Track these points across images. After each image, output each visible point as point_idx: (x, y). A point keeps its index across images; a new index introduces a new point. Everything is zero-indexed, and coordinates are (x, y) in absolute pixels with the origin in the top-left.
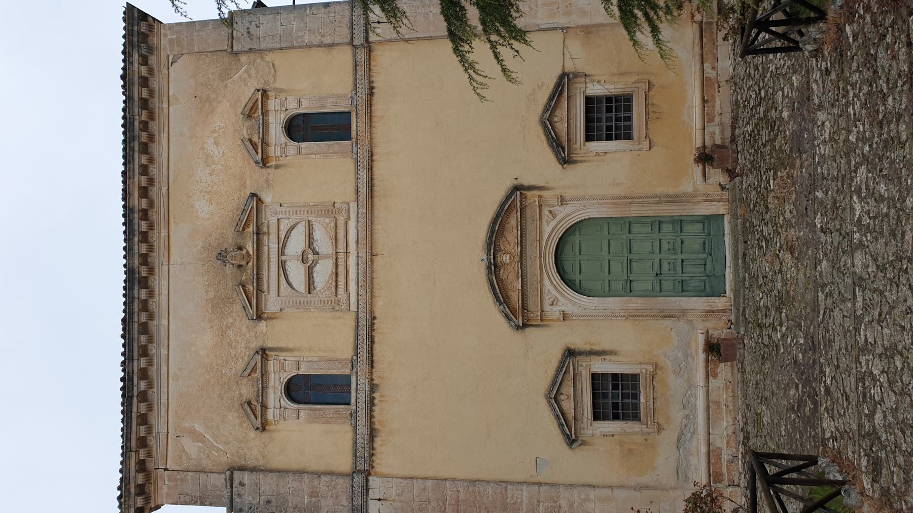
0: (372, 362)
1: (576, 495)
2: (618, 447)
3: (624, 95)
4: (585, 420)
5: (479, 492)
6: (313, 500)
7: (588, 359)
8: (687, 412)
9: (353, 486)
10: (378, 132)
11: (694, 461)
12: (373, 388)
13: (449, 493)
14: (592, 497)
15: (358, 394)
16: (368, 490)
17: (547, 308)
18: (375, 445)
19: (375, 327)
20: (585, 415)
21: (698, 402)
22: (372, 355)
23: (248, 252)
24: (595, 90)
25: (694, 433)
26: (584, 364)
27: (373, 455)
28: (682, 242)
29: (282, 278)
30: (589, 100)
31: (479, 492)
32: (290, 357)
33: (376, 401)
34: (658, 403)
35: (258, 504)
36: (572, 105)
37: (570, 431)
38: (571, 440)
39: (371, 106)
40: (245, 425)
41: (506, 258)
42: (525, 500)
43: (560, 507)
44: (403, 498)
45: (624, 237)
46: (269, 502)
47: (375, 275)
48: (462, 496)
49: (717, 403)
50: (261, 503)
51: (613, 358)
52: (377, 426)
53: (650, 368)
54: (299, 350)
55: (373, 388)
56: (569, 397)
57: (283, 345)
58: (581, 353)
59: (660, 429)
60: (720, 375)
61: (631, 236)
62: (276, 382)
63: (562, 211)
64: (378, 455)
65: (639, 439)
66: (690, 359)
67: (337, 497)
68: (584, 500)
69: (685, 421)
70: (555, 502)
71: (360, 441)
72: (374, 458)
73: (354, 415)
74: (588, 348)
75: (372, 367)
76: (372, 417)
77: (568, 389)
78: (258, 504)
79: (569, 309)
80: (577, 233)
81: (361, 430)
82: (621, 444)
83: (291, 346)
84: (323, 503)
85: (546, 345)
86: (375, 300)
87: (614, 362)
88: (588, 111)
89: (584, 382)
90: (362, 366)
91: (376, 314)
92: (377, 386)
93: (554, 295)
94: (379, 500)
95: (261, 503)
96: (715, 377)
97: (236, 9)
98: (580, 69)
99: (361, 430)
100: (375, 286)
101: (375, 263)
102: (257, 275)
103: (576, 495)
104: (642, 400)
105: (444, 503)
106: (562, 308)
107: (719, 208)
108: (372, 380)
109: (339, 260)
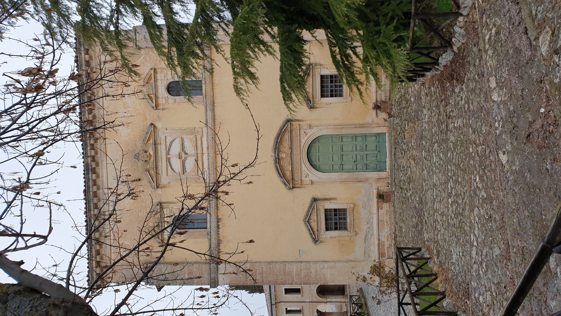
0: (218, 207)
1: (318, 267)
8: (369, 226)
10: (217, 91)
11: (372, 248)
12: (218, 220)
14: (326, 267)
16: (218, 270)
17: (304, 179)
23: (150, 154)
33: (220, 227)
34: (356, 221)
41: (284, 155)
48: (264, 270)
49: (383, 221)
52: (221, 239)
53: (352, 206)
55: (218, 220)
56: (314, 221)
58: (320, 200)
59: (356, 234)
61: (342, 143)
65: (347, 239)
73: (209, 234)
74: (323, 197)
75: (218, 210)
76: (218, 234)
79: (314, 179)
81: (213, 241)
85: (303, 197)
87: (335, 203)
92: (220, 219)
93: (307, 172)
96: (382, 209)
98: (318, 62)
99: (213, 241)
103: (318, 267)
104: (348, 220)
106: (311, 179)
107: (384, 130)
108: (218, 216)
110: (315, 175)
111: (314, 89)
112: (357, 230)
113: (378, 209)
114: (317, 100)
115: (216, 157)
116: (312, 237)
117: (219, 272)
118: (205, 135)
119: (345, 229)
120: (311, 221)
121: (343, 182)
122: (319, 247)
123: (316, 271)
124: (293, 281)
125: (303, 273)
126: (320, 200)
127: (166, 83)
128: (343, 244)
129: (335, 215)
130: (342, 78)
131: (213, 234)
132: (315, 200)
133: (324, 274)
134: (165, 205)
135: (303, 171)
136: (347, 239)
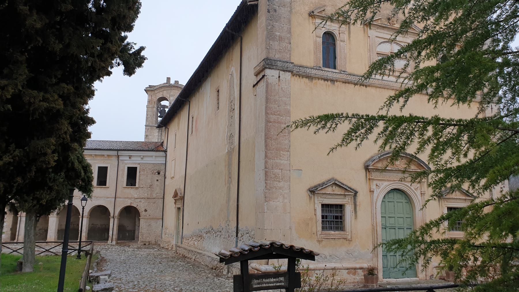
0: (345, 83)
1: (286, 191)
2: (309, 217)
3: (344, 226)
4: (322, 199)
5: (285, 136)
6: (278, 38)
7: (353, 203)
8: (328, 257)
9: (287, 62)
12: (333, 81)
14: (286, 201)
15: (329, 73)
16: (284, 71)
17: (375, 182)
18: (304, 78)
19: (362, 87)
20: (325, 200)
21: (333, 264)
22: (349, 83)
23: (395, 24)
24: (348, 210)
27: (299, 77)
29: (383, 40)
30: (341, 207)
31: (285, 136)
32: (345, 37)
33: (326, 82)
34: (332, 241)
35: (274, 4)
36: (462, 201)
37: (319, 190)
38: (313, 191)
40: (312, 5)
42: (282, 162)
45: (405, 226)
46: (275, 11)
47: (386, 90)
50: (275, 6)
51: (353, 217)
52: (314, 81)
53: (349, 237)
54: (350, 43)
55: (333, 81)
56: (333, 191)
57: (352, 34)
58: (355, 199)
59: (319, 242)
60: (348, 275)
61: (405, 229)
62: (333, 27)
63: (418, 193)
64: (299, 80)
65: (314, 230)
66: (354, 259)
67: (280, 52)
68: (284, 196)
69: (323, 256)
70: (282, 179)
71: (308, 71)
72: (298, 77)
73: (319, 69)
74: (358, 204)
75: (343, 82)
76: (319, 79)
77: (338, 191)
78: (274, 4)
79: (375, 194)
80: (406, 201)
81: (314, 72)
83: (351, 39)
84: (276, 43)
85: (356, 180)
86: (375, 88)
87: (351, 218)
88: (337, 206)
89: (339, 200)
90: (344, 77)
91: (368, 88)
92: (334, 84)
93: (384, 185)
94: (279, 77)
95: (275, 6)
96: (348, 273)
99: (314, 72)
100: (381, 89)
101: (391, 91)
102: (386, 27)
103: (286, 191)
104: (333, 232)
105: (278, 115)
106: (375, 190)
108: (337, 81)
110: (380, 193)
111: (458, 201)
112: (324, 243)
114: (446, 203)
115: (393, 89)
116: (319, 185)
117: (281, 72)
119: (323, 228)
120: (334, 187)
121: (374, 230)
122: (304, 194)
123: (280, 188)
124: (270, 159)
126: (355, 199)
127: (336, 33)
129: (337, 217)
131: (319, 73)
132: (356, 193)
133: (277, 198)
134: (347, 28)
135: (383, 182)
136: (314, 230)
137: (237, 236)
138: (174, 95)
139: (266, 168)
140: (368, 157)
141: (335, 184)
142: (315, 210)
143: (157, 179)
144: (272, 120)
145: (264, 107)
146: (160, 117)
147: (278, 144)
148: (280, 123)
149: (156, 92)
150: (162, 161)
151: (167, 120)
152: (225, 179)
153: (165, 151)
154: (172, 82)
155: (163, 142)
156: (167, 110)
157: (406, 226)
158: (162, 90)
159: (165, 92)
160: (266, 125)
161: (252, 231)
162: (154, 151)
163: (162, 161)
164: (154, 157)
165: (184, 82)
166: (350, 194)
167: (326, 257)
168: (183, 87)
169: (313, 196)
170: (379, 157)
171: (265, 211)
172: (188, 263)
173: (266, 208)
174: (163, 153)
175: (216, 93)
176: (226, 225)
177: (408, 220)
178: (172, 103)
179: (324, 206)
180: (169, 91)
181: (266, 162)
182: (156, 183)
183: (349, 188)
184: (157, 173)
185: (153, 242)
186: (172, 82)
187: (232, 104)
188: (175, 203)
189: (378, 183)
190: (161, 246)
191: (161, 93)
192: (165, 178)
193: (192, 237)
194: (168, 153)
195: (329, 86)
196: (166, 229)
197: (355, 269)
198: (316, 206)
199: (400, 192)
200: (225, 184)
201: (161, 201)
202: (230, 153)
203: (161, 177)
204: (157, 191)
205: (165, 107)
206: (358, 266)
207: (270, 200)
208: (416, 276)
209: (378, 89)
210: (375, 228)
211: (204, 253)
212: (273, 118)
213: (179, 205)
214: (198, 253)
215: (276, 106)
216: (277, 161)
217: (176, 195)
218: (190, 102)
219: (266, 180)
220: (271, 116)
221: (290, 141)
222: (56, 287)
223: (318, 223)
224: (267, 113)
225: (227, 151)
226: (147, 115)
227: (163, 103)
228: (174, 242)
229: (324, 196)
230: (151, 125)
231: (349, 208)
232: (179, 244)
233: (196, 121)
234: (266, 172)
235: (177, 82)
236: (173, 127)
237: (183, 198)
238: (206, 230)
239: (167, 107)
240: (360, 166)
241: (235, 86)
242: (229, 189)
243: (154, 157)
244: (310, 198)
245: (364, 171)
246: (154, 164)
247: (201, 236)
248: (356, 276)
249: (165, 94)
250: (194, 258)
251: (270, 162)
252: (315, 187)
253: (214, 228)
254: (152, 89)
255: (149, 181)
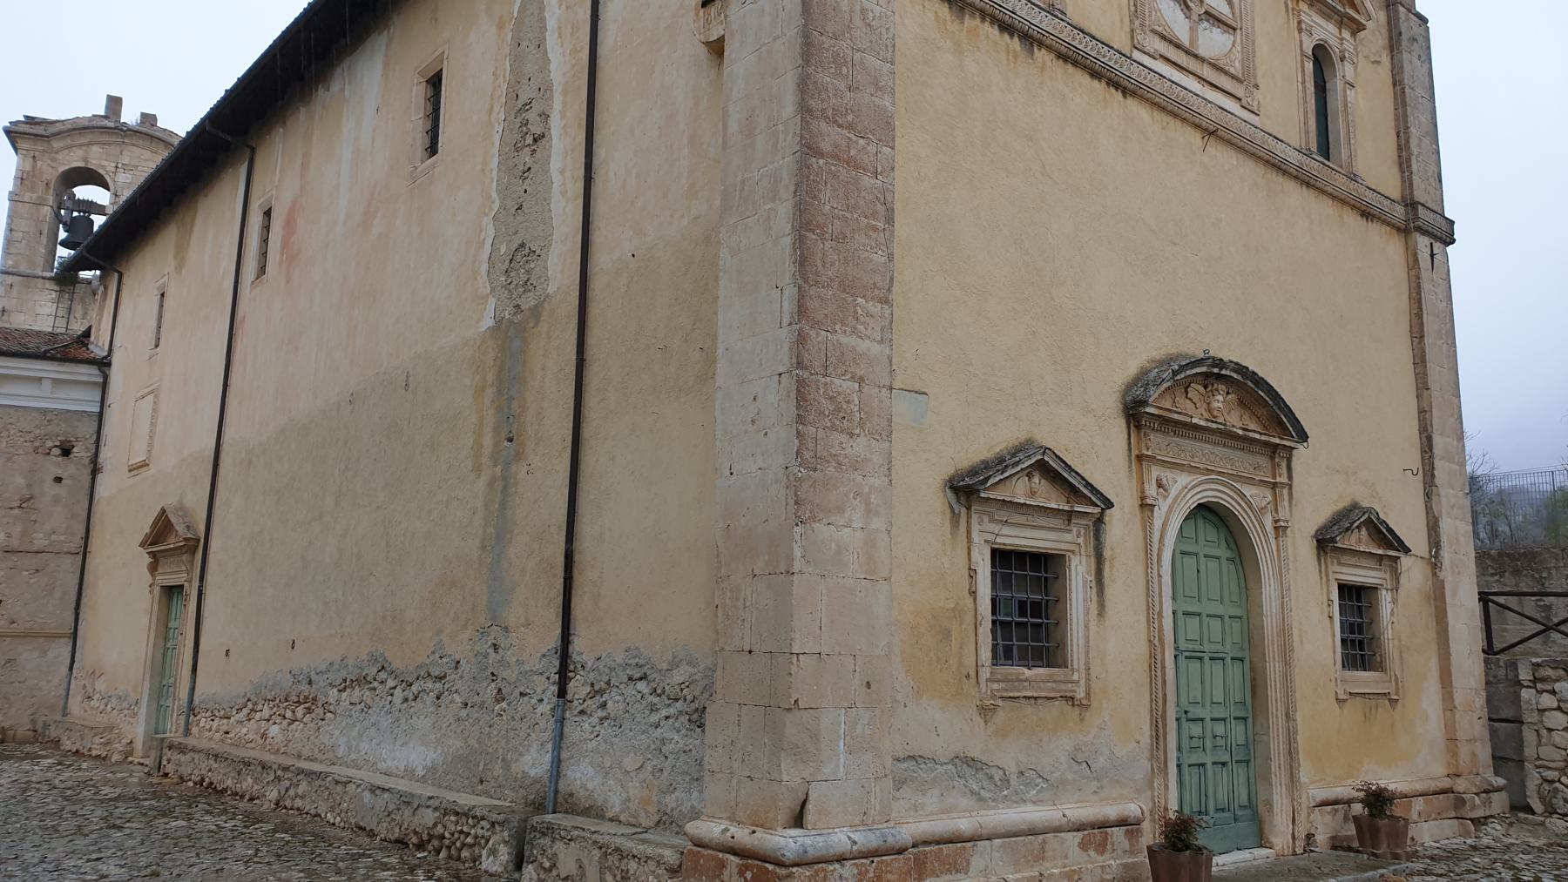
5: (875, 229)
10: (1327, 208)
11: (931, 800)
13: (872, 149)
14: (877, 524)
17: (1156, 471)
20: (1006, 530)
21: (1030, 807)
22: (1075, 64)
25: (981, 799)
26: (1081, 540)
28: (1223, 764)
34: (1029, 709)
36: (1372, 563)
38: (966, 490)
39: (1353, 207)
41: (1219, 401)
42: (863, 345)
43: (852, 435)
44: (857, 22)
48: (867, 181)
49: (1040, 857)
53: (1080, 694)
56: (1033, 494)
59: (986, 711)
68: (867, 503)
74: (1107, 553)
82: (957, 612)
85: (1101, 454)
97: (165, 154)
98: (1403, 579)
103: (876, 481)
107: (1281, 836)
109: (1183, 54)
112: (1000, 716)
113: (1079, 828)
118: (1245, 115)
122: (936, 501)
124: (816, 324)
125: (849, 386)
128: (946, 635)
130: (486, 794)
133: (840, 510)
137: (562, 693)
138: (133, 170)
139: (800, 364)
140: (1132, 369)
141: (1042, 468)
142: (972, 573)
143: (59, 472)
144: (826, 146)
145: (789, 81)
146: (64, 244)
147: (846, 262)
148: (857, 167)
149: (56, 144)
150: (86, 401)
151: (113, 247)
152: (478, 445)
153: (104, 364)
154: (129, 116)
155: (87, 334)
156: (99, 221)
157: (1229, 650)
158: (83, 140)
159: (96, 149)
160: (803, 168)
161: (674, 665)
162: (53, 359)
163: (86, 401)
164: (47, 385)
165: (181, 120)
166: (1090, 510)
167: (1006, 780)
168: (176, 142)
169: (963, 510)
170: (1175, 373)
171: (797, 567)
172: (252, 819)
173: (798, 553)
174: (94, 370)
175: (419, 92)
176: (483, 646)
177: (1236, 625)
178: (126, 194)
179: (1001, 557)
180: (115, 150)
181: (801, 339)
182: (51, 489)
183: (1088, 485)
184: (57, 451)
185: (22, 732)
186: (129, 116)
187: (532, 116)
188: (153, 568)
189: (1167, 475)
190: (67, 745)
191: (79, 153)
192: (95, 471)
193: (249, 706)
194: (116, 373)
195: (1015, 57)
196: (94, 674)
197: (1103, 825)
198: (975, 556)
199: (1213, 518)
200: (477, 469)
201: (70, 565)
202: (512, 336)
203: (74, 469)
204: (56, 523)
205: (91, 207)
206: (1112, 812)
207: (814, 519)
208: (1262, 841)
209: (1158, 115)
210: (1159, 657)
211: (342, 772)
212: (830, 136)
213: (172, 575)
214: (301, 771)
215: (842, 85)
216: (844, 340)
217: (162, 528)
218: (253, 150)
219: (800, 419)
220: (823, 126)
221: (891, 257)
222: (85, 160)
223: (980, 630)
224: (804, 109)
225: (490, 323)
226: (10, 230)
227: (84, 192)
228: (137, 730)
229: (1002, 515)
230: (23, 268)
231: (1080, 568)
232: (173, 732)
233: (290, 224)
234: (801, 383)
235: (148, 119)
236: (149, 272)
237: (197, 547)
238: (343, 674)
239: (100, 210)
240: (1111, 404)
241: (551, 41)
242: (503, 488)
243: (47, 385)
244: (955, 518)
245: (1122, 422)
246: (44, 411)
247: (309, 703)
248: (1107, 855)
249: (96, 158)
250: (273, 794)
251: (817, 337)
252: (973, 472)
253: (397, 664)
254: (39, 130)
255: (20, 481)
